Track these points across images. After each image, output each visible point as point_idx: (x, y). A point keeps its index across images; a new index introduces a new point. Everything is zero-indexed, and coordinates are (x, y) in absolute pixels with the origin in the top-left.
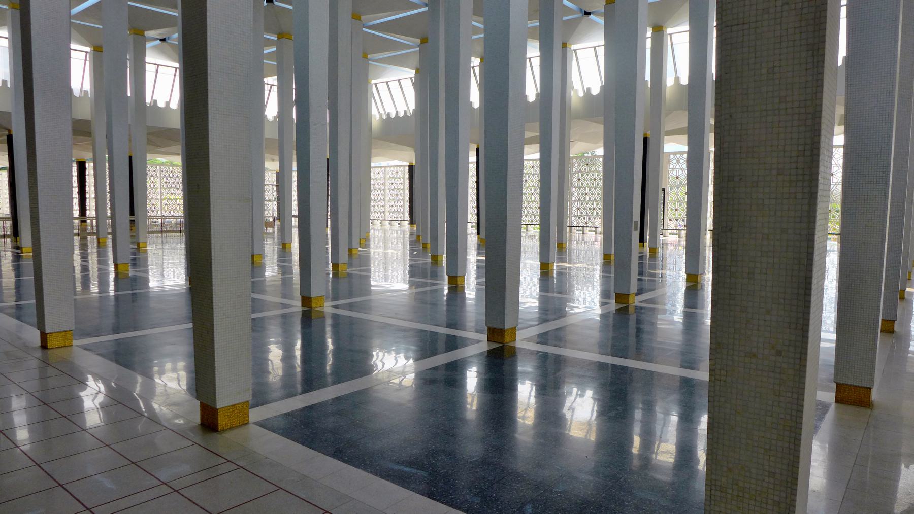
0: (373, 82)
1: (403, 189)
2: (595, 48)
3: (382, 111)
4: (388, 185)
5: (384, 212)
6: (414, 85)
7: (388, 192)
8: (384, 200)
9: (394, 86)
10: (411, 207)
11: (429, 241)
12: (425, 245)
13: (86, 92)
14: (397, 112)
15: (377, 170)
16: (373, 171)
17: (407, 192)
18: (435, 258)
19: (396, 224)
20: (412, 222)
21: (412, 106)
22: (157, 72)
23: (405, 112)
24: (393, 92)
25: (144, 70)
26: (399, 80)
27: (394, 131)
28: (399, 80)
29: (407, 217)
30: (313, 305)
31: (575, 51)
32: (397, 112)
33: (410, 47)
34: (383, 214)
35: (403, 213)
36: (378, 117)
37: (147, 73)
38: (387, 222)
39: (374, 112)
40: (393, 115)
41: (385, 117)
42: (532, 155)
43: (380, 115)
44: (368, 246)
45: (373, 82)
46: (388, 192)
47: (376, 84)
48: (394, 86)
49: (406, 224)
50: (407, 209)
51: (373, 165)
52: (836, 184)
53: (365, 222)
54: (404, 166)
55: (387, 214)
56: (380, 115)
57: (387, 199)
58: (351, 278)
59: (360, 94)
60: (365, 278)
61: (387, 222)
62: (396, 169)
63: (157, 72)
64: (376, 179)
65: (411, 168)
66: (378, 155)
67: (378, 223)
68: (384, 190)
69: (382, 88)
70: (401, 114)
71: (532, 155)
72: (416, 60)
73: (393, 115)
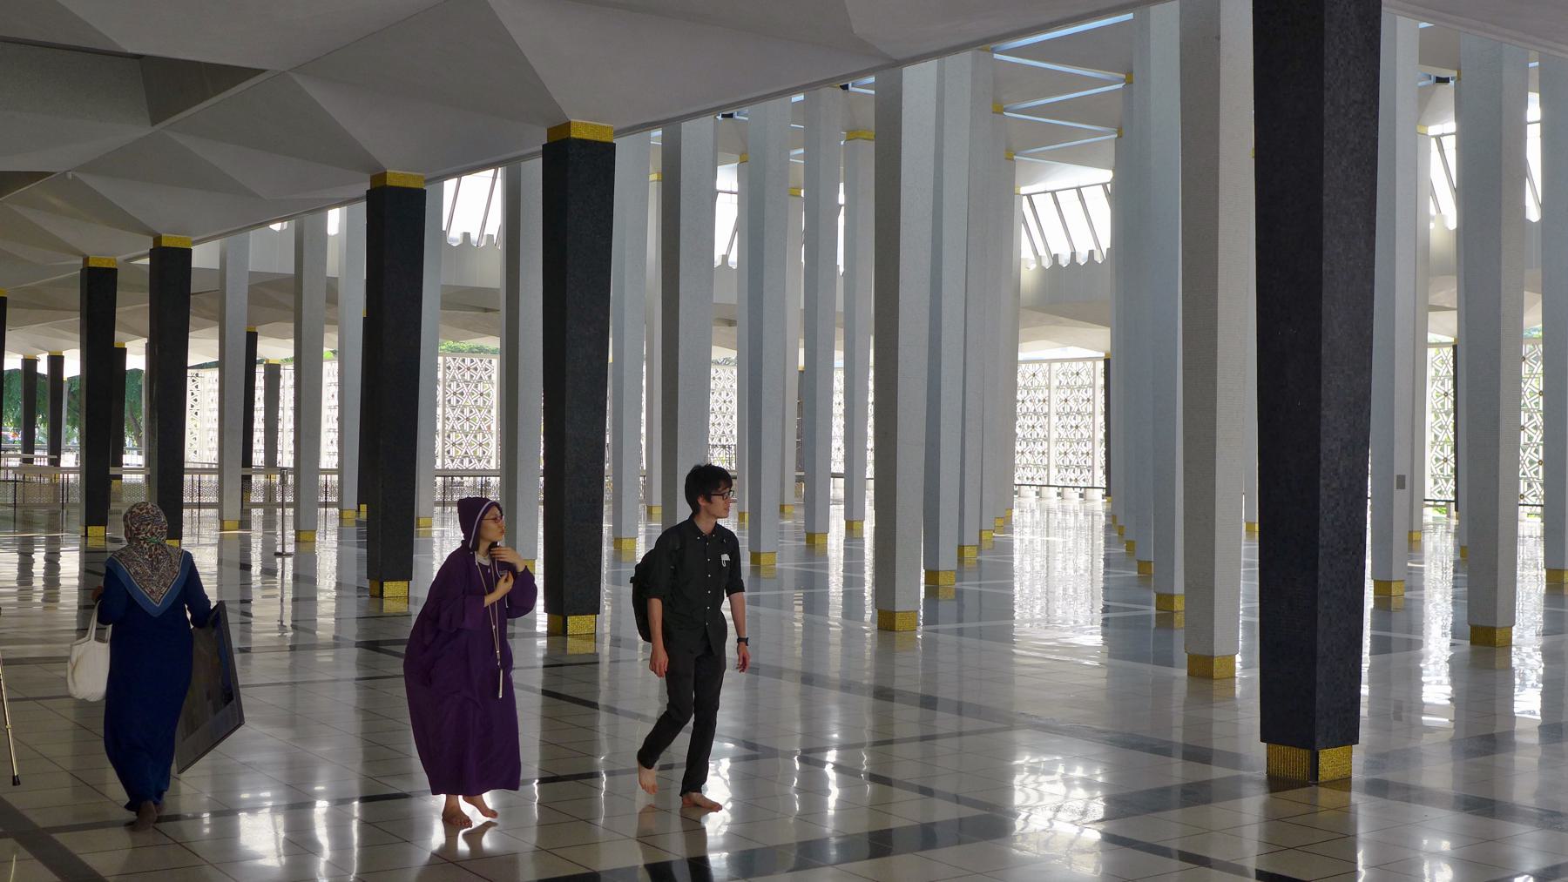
0: (1024, 190)
1: (1092, 414)
3: (1042, 252)
4: (1055, 405)
5: (1047, 468)
6: (1108, 195)
7: (1054, 419)
8: (1047, 439)
9: (1069, 200)
10: (1108, 454)
11: (1179, 587)
12: (1165, 600)
13: (490, 237)
14: (1073, 255)
15: (1031, 368)
16: (1021, 368)
17: (1100, 419)
19: (1073, 495)
21: (1106, 242)
23: (1091, 253)
24: (1067, 212)
26: (1078, 189)
27: (1066, 293)
28: (1078, 189)
29: (1100, 479)
30: (941, 582)
32: (1073, 255)
33: (1109, 83)
34: (1043, 473)
35: (1091, 468)
36: (1033, 266)
39: (1026, 252)
40: (1064, 261)
41: (1047, 263)
42: (329, 456)
44: (1011, 531)
45: (1024, 190)
46: (1054, 419)
47: (1029, 196)
48: (1069, 200)
49: (1099, 493)
51: (1021, 356)
52: (1532, 375)
53: (1007, 492)
55: (1054, 471)
57: (1054, 436)
59: (996, 216)
62: (1075, 367)
65: (1107, 362)
67: (1029, 493)
68: (1047, 415)
69: (1044, 204)
70: (1082, 259)
71: (329, 456)
72: (1110, 151)
73: (1064, 261)
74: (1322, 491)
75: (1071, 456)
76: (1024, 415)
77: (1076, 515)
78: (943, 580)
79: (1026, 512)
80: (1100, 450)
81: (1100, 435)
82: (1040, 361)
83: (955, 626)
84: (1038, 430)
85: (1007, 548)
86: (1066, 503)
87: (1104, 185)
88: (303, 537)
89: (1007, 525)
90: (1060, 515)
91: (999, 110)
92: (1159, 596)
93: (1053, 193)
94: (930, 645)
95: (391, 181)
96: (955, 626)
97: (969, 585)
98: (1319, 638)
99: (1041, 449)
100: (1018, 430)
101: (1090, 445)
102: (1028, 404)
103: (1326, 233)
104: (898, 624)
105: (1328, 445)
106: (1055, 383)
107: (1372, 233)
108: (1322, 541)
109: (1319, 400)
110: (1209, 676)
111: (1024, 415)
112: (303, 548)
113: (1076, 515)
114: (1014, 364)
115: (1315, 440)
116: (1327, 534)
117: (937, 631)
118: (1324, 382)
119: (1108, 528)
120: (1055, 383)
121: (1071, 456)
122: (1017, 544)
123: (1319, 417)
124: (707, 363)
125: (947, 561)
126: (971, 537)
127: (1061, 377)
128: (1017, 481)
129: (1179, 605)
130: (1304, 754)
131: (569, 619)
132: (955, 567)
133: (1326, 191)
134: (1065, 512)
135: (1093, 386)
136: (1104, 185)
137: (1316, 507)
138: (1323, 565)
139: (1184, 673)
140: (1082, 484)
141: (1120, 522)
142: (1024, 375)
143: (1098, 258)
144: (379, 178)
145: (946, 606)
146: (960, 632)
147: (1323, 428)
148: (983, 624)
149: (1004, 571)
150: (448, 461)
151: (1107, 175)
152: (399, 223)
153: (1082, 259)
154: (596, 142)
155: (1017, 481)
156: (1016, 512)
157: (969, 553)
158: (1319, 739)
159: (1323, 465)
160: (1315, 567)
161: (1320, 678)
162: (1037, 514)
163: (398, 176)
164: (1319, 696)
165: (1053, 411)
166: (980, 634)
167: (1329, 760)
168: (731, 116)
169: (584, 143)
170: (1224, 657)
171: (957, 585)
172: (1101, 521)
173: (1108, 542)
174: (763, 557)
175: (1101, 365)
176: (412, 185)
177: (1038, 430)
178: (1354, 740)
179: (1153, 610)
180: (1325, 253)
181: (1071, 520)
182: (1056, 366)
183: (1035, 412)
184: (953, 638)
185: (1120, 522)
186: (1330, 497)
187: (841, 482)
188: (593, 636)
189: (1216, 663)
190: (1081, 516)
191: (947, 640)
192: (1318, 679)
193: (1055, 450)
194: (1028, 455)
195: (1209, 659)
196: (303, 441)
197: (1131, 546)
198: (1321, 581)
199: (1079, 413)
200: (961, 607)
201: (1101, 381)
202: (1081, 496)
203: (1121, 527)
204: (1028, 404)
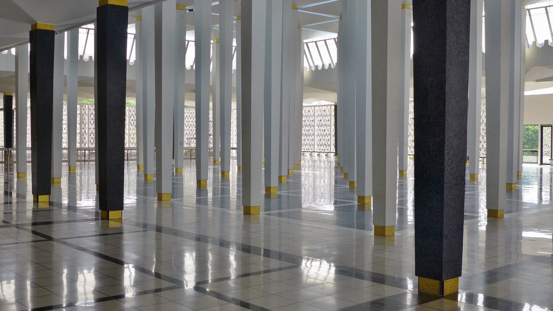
1: (330, 126)
2: (546, 7)
3: (312, 64)
5: (314, 145)
6: (336, 43)
7: (316, 127)
8: (314, 135)
9: (321, 45)
10: (336, 140)
12: (352, 184)
14: (323, 65)
15: (308, 109)
16: (304, 109)
17: (333, 127)
18: (361, 199)
19: (323, 155)
20: (336, 154)
21: (335, 61)
22: (547, 13)
23: (330, 64)
24: (321, 50)
25: (127, 38)
26: (325, 40)
27: (320, 79)
28: (325, 40)
29: (333, 149)
31: (529, 10)
32: (323, 65)
34: (312, 147)
35: (330, 145)
37: (128, 39)
38: (316, 154)
39: (306, 64)
40: (320, 68)
41: (313, 69)
43: (310, 67)
45: (305, 41)
46: (316, 127)
47: (307, 43)
48: (321, 45)
49: (332, 154)
50: (333, 142)
51: (304, 104)
53: (298, 154)
54: (331, 105)
55: (316, 147)
56: (310, 67)
58: (284, 194)
59: (295, 51)
60: (298, 203)
61: (316, 154)
63: (547, 13)
64: (306, 116)
65: (336, 106)
66: (308, 97)
67: (308, 154)
68: (314, 126)
69: (312, 46)
70: (326, 67)
73: (320, 68)
74: (446, 156)
75: (322, 141)
76: (305, 126)
77: (324, 163)
78: (272, 191)
79: (306, 161)
80: (333, 139)
81: (333, 133)
82: (311, 106)
83: (277, 211)
84: (311, 131)
85: (299, 176)
86: (321, 158)
87: (335, 39)
88: (20, 175)
89: (299, 167)
90: (318, 163)
91: (295, 8)
92: (359, 197)
93: (316, 42)
94: (267, 222)
95: (39, 27)
96: (277, 211)
97: (284, 193)
98: (444, 227)
99: (311, 138)
100: (303, 131)
101: (329, 137)
102: (307, 122)
103: (448, 32)
104: (252, 211)
105: (449, 134)
106: (317, 114)
107: (468, 32)
108: (446, 180)
109: (444, 112)
110: (383, 235)
111: (305, 126)
112: (20, 179)
113: (324, 163)
114: (301, 107)
115: (443, 131)
116: (448, 177)
117: (270, 214)
118: (447, 104)
119: (336, 168)
120: (317, 114)
121: (322, 141)
122: (303, 174)
123: (444, 120)
124: (183, 107)
125: (274, 183)
126: (284, 173)
127: (319, 131)
128: (303, 150)
129: (356, 185)
130: (437, 283)
131: (110, 212)
132: (277, 185)
133: (448, 10)
134: (320, 161)
135: (330, 115)
136: (335, 39)
137: (443, 164)
138: (446, 192)
139: (372, 233)
140: (326, 151)
141: (342, 165)
142: (305, 112)
143: (332, 67)
144: (34, 25)
145: (274, 202)
146: (280, 215)
147: (446, 126)
148: (290, 210)
149: (298, 185)
150: (90, 144)
151: (335, 35)
152: (43, 45)
153: (326, 67)
154: (119, 6)
155: (303, 150)
156: (302, 162)
157: (284, 179)
158: (444, 276)
159: (446, 144)
160: (442, 193)
161: (444, 247)
162: (310, 162)
163: (42, 25)
164: (444, 255)
165: (316, 124)
166: (289, 216)
167: (448, 284)
168: (192, 10)
169: (114, 6)
170: (390, 227)
171: (279, 193)
172: (333, 165)
173: (336, 173)
174: (202, 182)
175: (333, 107)
176: (48, 28)
177: (311, 131)
178: (459, 274)
179: (356, 203)
180: (448, 41)
181: (322, 164)
182: (317, 108)
183: (309, 125)
184: (277, 218)
185: (342, 165)
186: (449, 159)
187: (234, 151)
188: (120, 220)
189: (386, 229)
190: (326, 163)
191: (274, 219)
192: (444, 247)
193: (317, 139)
194: (307, 141)
195: (383, 228)
196: (19, 137)
197: (346, 175)
198: (445, 200)
199: (325, 125)
200: (280, 203)
201: (333, 113)
202: (326, 155)
203: (341, 168)
204: (307, 122)
